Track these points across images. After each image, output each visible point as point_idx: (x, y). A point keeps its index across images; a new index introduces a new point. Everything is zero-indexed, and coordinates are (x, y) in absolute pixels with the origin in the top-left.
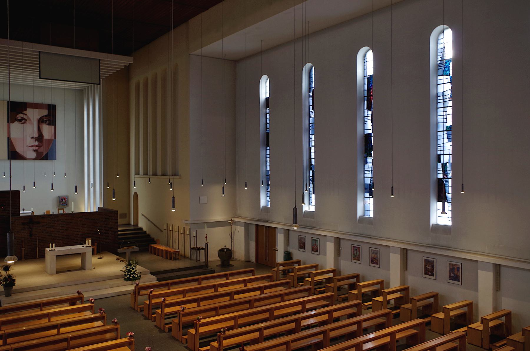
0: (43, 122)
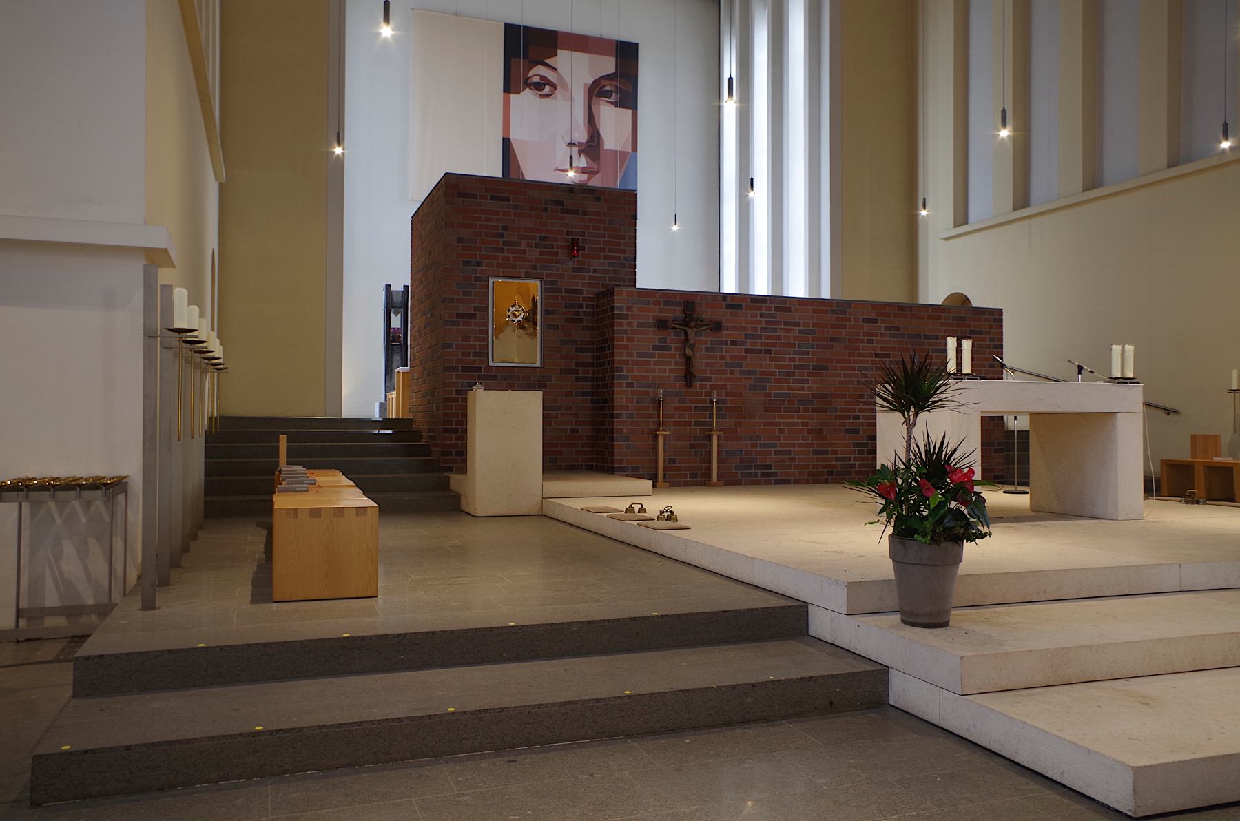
0: (607, 95)
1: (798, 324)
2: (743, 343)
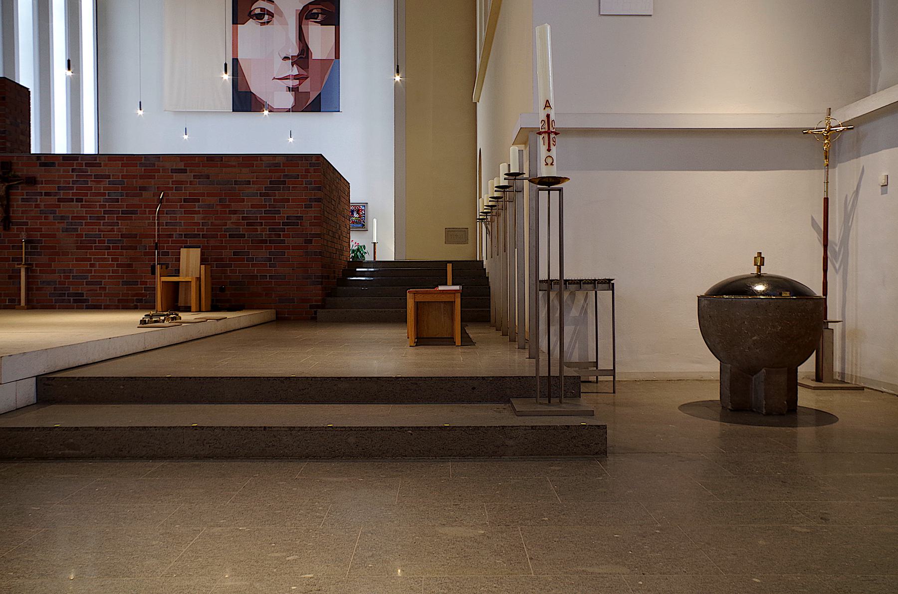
1: (108, 177)
2: (56, 194)
